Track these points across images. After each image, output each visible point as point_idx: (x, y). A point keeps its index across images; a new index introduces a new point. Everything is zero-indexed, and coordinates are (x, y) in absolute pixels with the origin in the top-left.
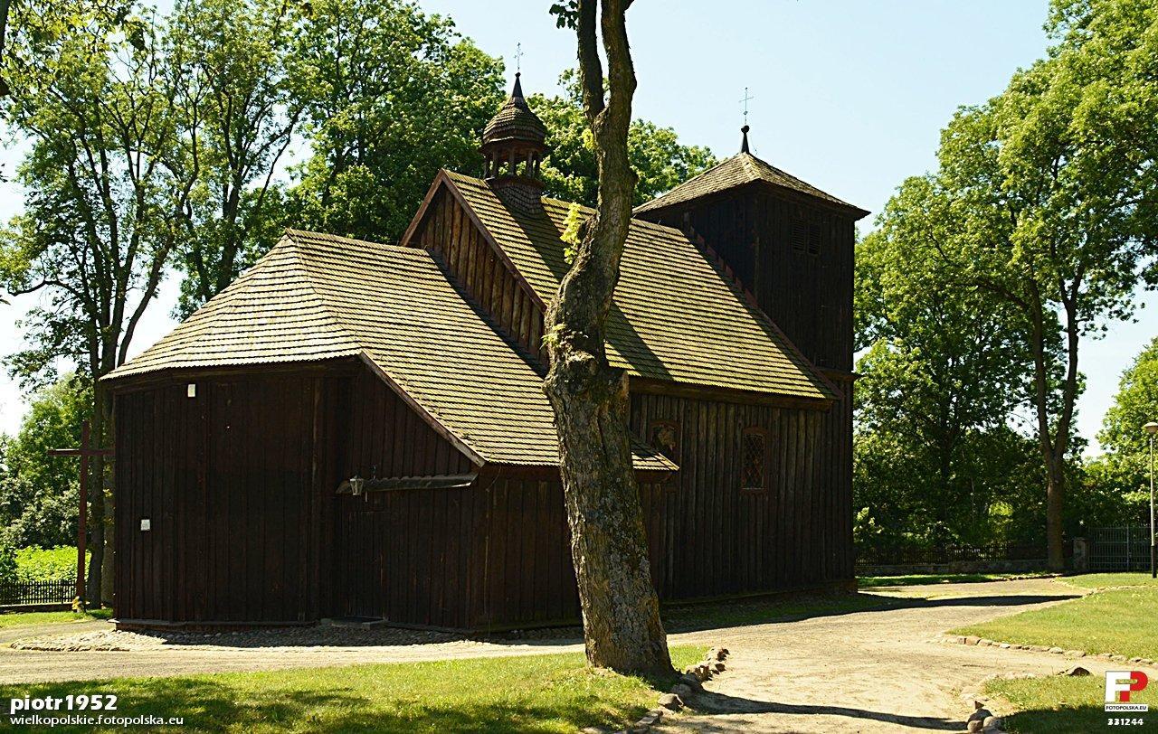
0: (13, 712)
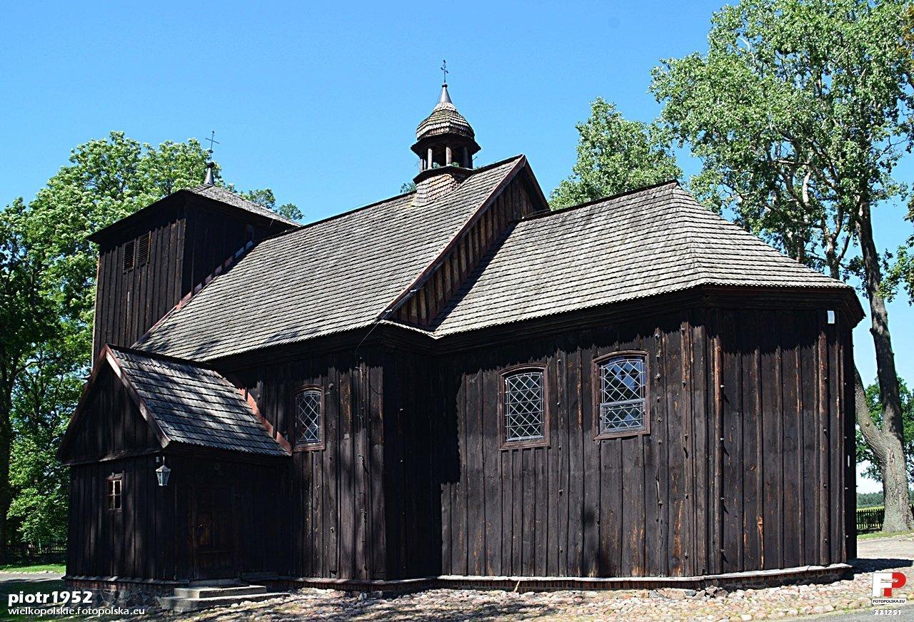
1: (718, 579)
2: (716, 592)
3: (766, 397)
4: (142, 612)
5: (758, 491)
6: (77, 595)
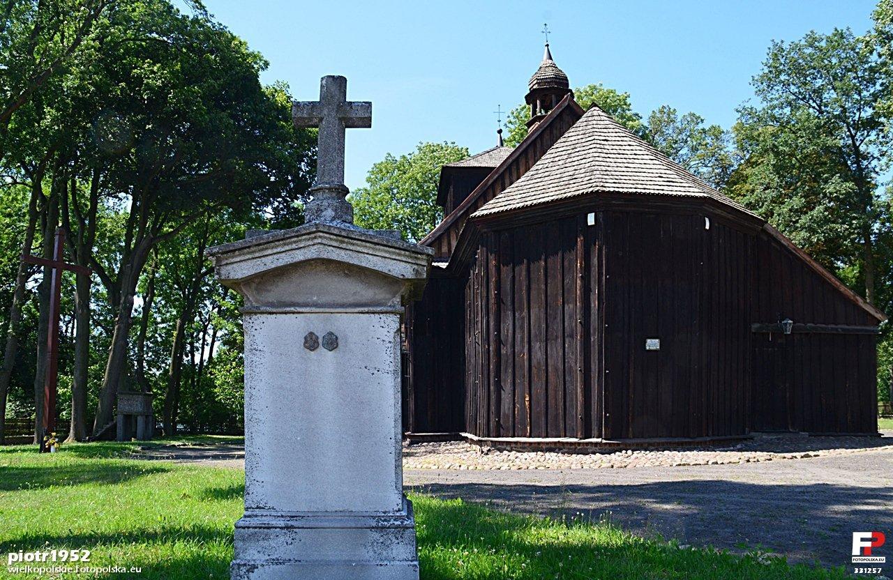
1: (492, 441)
2: (489, 450)
3: (550, 307)
4: (138, 570)
5: (526, 374)
6: (75, 553)
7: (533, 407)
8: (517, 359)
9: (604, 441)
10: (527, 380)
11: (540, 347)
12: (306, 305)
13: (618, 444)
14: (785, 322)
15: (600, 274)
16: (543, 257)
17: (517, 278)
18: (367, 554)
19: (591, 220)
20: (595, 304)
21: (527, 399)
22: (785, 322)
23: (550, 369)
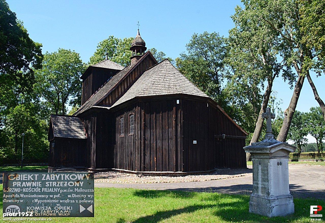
0: (14, 186)
1: (142, 173)
2: (141, 176)
7: (157, 161)
8: (151, 145)
9: (183, 173)
10: (155, 152)
11: (160, 142)
12: (277, 157)
13: (186, 173)
14: (223, 135)
15: (181, 120)
16: (161, 112)
17: (152, 118)
18: (287, 202)
19: (178, 102)
20: (179, 129)
21: (155, 159)
22: (223, 135)
23: (163, 149)
